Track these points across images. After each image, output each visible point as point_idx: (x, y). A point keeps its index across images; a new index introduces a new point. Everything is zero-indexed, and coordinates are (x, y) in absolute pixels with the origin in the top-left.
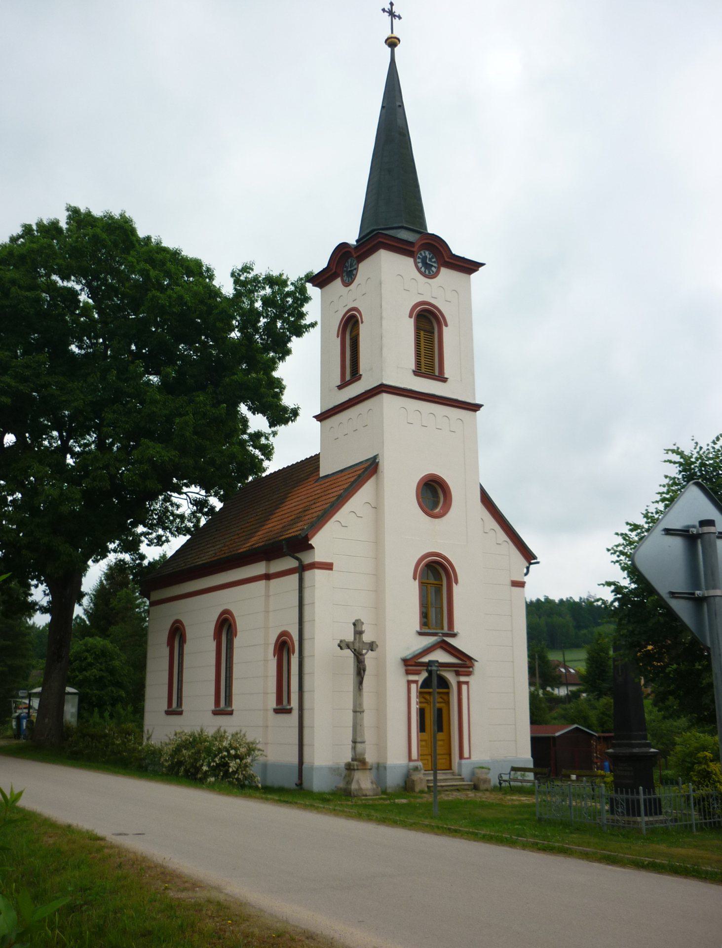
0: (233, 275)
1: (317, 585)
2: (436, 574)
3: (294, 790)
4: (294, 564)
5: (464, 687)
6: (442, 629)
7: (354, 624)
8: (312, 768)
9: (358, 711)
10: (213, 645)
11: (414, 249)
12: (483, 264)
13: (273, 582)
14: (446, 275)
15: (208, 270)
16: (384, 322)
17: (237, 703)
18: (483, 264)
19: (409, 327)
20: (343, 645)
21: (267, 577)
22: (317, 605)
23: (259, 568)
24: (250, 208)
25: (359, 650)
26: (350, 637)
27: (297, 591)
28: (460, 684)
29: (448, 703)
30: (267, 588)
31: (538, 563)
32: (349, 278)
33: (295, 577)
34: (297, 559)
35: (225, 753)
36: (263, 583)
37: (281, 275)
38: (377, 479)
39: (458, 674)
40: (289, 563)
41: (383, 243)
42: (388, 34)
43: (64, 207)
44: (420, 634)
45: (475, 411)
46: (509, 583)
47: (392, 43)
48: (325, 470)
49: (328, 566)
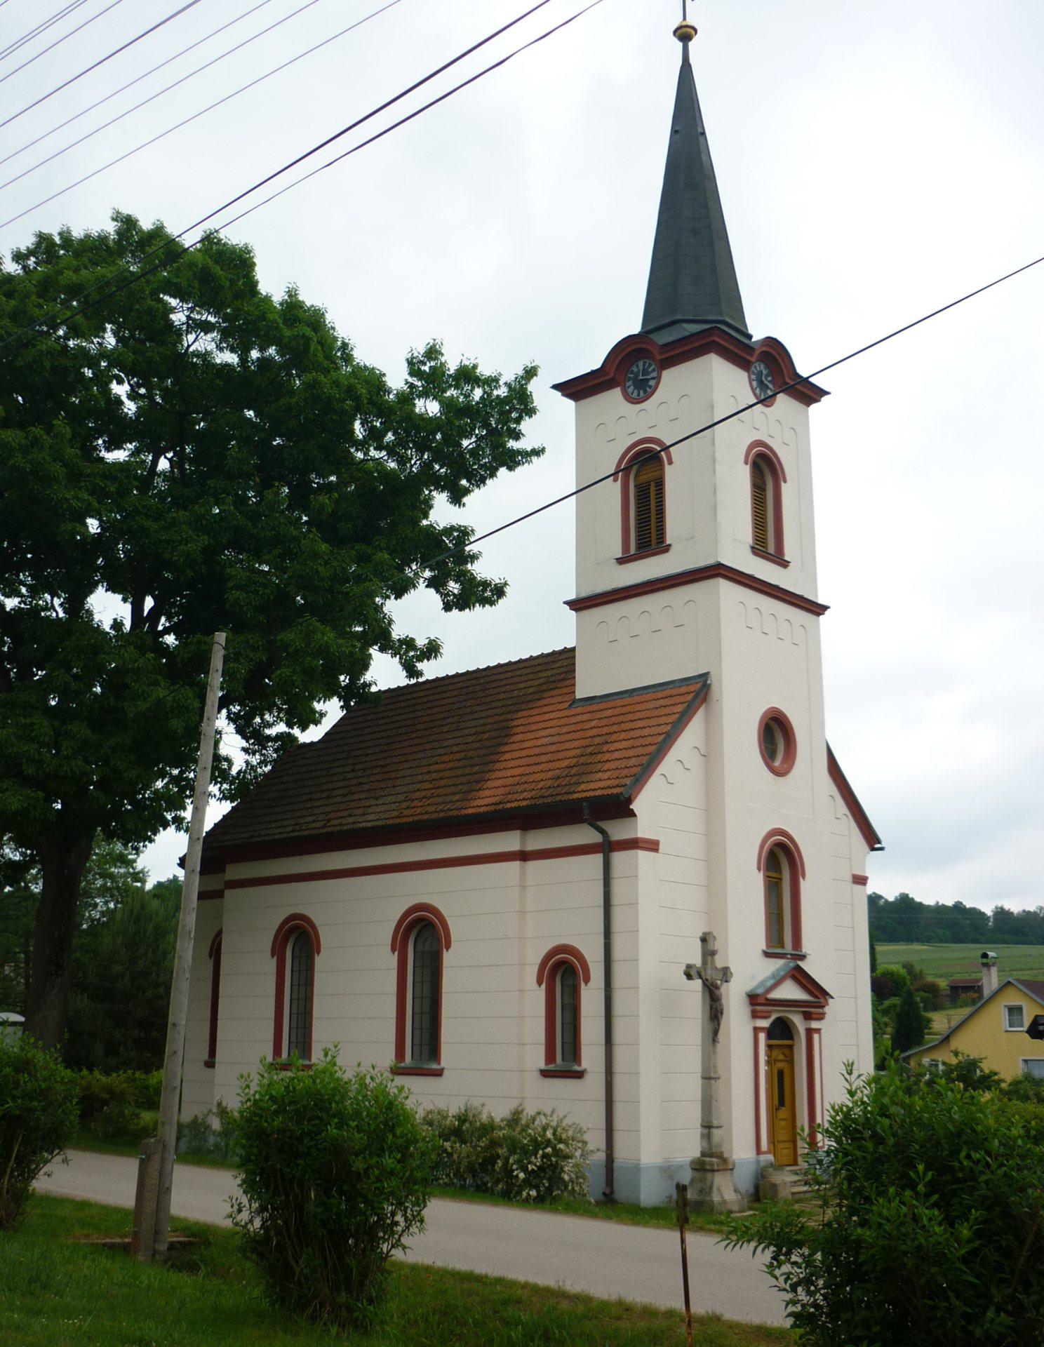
0: (410, 363)
1: (641, 874)
2: (781, 859)
3: (612, 1201)
4: (596, 838)
5: (816, 1037)
6: (783, 947)
7: (704, 940)
8: (636, 1169)
9: (709, 1078)
10: (393, 960)
11: (753, 359)
12: (828, 393)
13: (533, 865)
14: (783, 402)
15: (345, 345)
16: (718, 467)
17: (447, 1057)
18: (828, 393)
19: (744, 476)
20: (693, 973)
21: (524, 856)
22: (641, 906)
23: (510, 841)
24: (446, 257)
25: (710, 979)
26: (697, 961)
27: (602, 882)
28: (810, 1032)
29: (791, 1062)
30: (523, 873)
31: (882, 849)
32: (642, 390)
33: (598, 858)
34: (602, 832)
35: (549, 1150)
36: (516, 865)
37: (475, 367)
38: (707, 709)
39: (808, 1017)
40: (584, 835)
41: (718, 344)
42: (677, 21)
43: (110, 213)
44: (767, 954)
45: (819, 614)
46: (849, 878)
47: (685, 34)
48: (588, 684)
49: (653, 846)
